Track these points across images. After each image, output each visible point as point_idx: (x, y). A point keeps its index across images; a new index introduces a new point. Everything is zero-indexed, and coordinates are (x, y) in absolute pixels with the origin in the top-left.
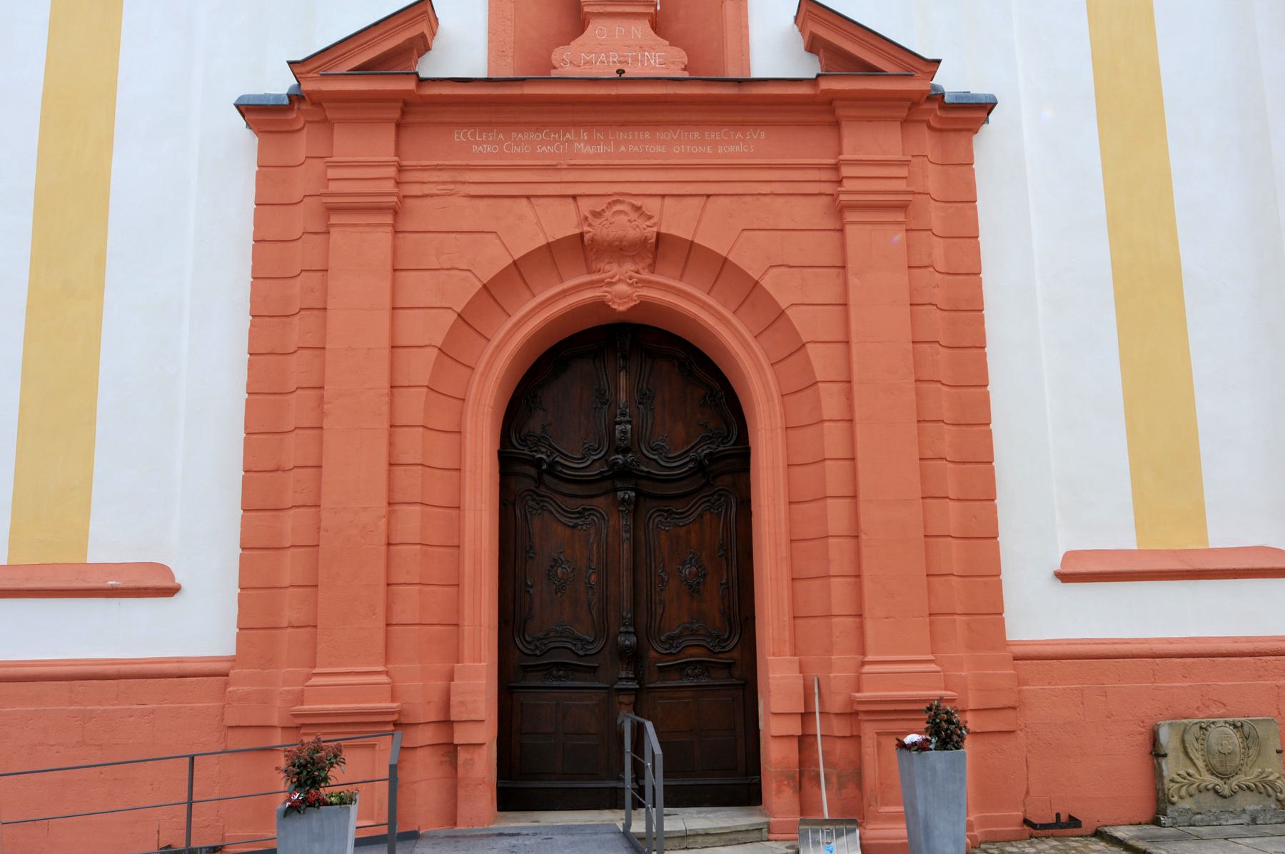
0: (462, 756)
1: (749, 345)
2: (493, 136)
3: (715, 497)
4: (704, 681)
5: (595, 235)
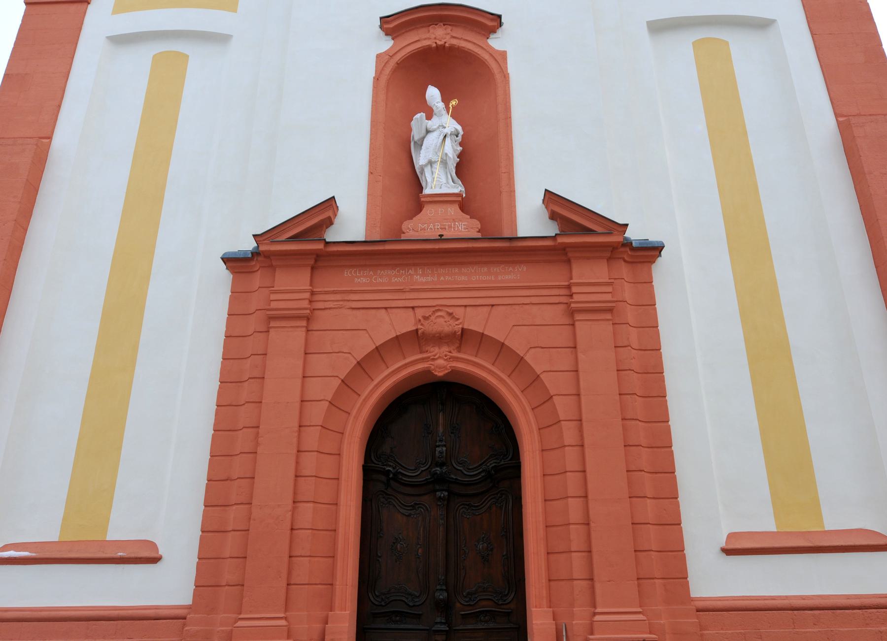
3: (499, 495)
4: (491, 625)
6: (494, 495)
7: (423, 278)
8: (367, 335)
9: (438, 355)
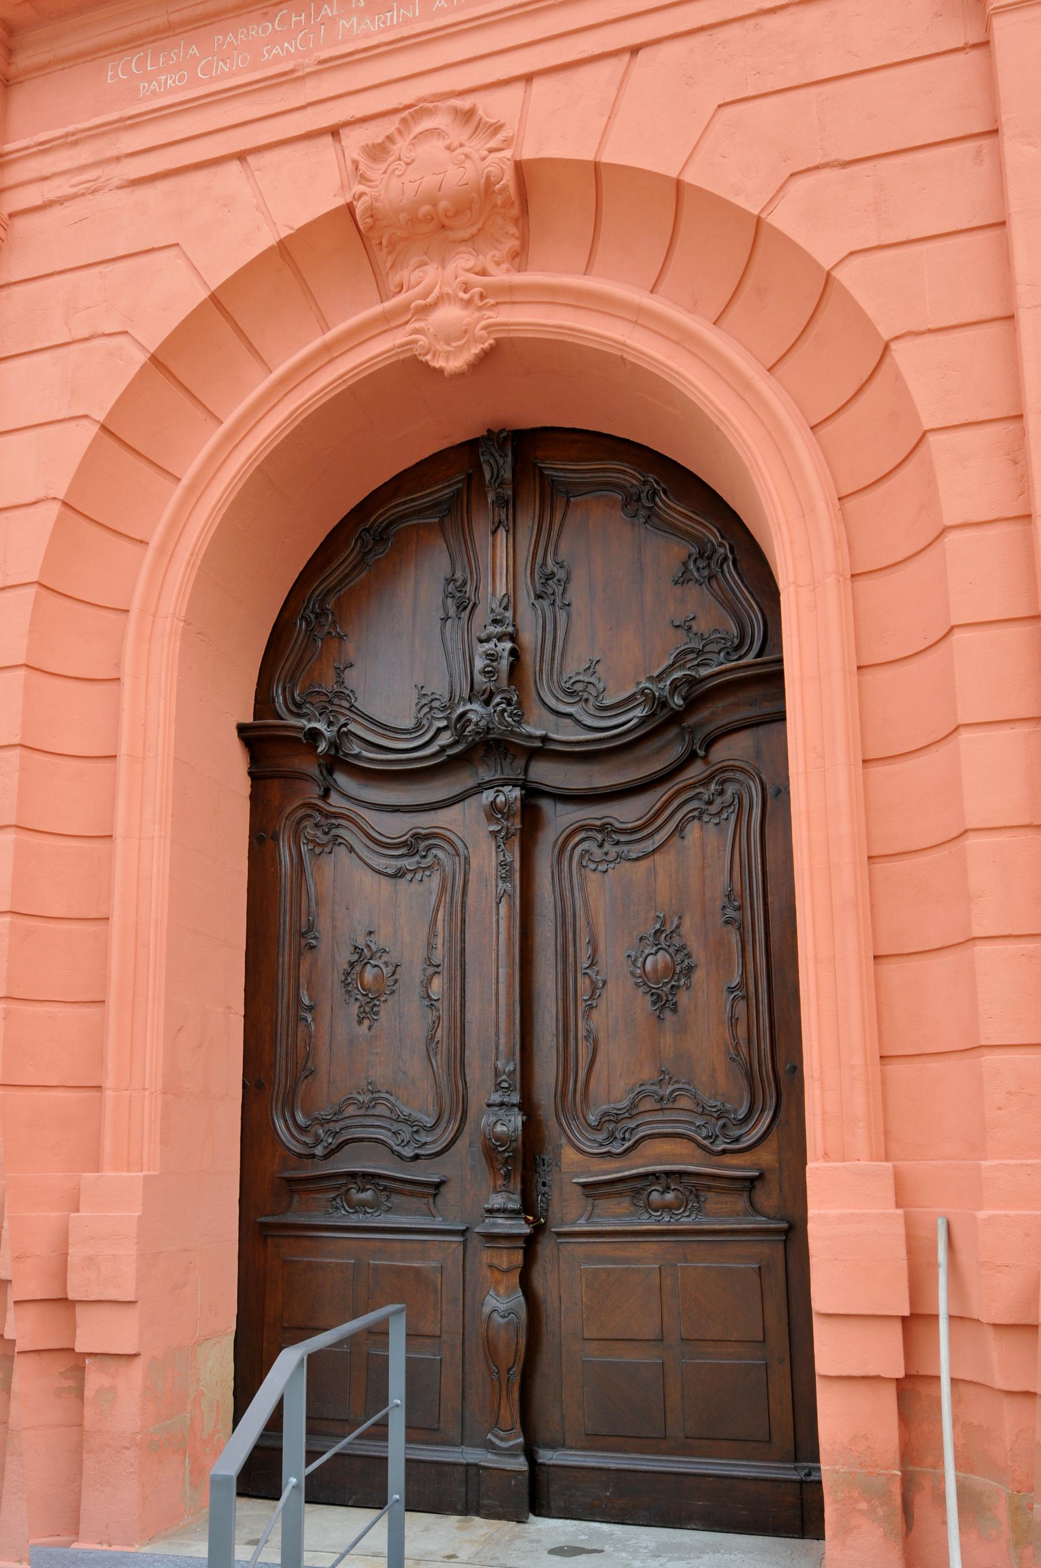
0: (95, 1379)
1: (749, 386)
2: (177, 55)
3: (713, 787)
4: (686, 1221)
5: (377, 200)
6: (693, 786)
7: (373, 22)
8: (181, 262)
9: (437, 289)
